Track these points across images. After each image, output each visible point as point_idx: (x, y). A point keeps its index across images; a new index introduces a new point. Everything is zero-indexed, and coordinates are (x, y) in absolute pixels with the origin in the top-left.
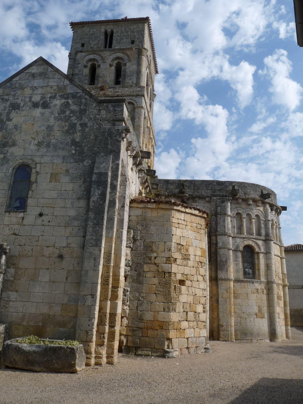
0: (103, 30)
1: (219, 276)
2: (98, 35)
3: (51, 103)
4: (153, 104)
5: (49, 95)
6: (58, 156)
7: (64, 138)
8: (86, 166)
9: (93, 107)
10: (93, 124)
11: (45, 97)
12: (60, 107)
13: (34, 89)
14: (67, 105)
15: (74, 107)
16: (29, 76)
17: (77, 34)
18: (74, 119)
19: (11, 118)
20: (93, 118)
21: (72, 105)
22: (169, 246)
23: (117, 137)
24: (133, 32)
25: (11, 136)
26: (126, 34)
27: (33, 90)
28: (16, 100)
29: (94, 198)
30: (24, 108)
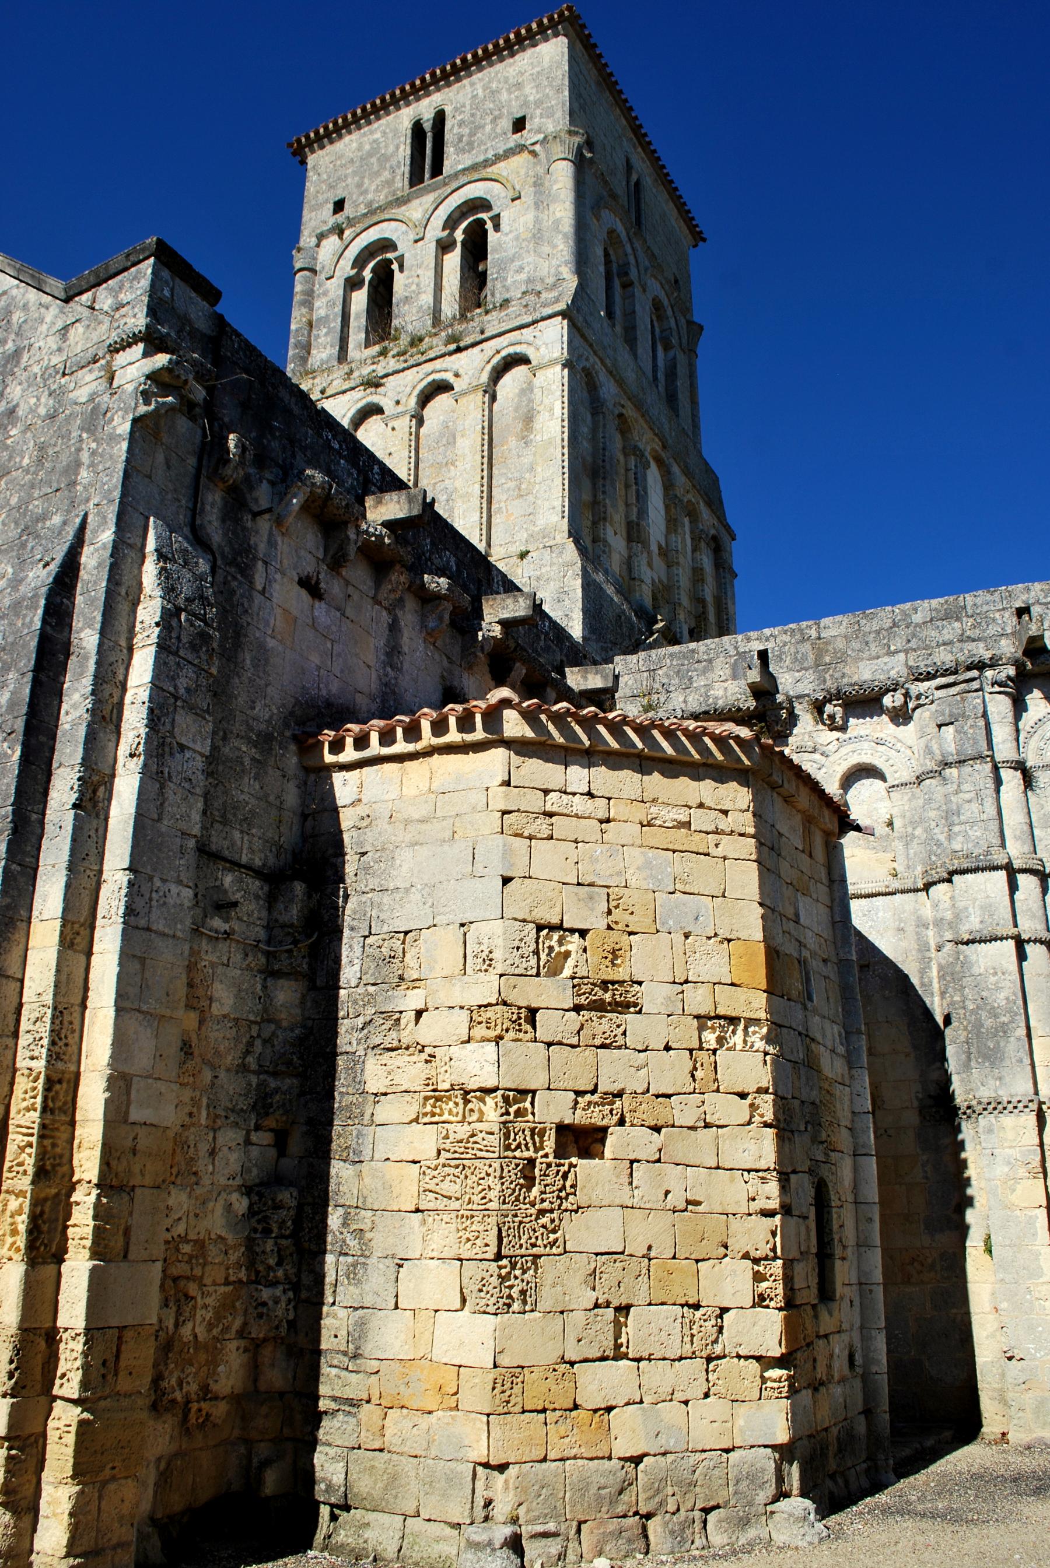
2: (391, 148)
4: (692, 375)
20: (39, 376)
22: (486, 941)
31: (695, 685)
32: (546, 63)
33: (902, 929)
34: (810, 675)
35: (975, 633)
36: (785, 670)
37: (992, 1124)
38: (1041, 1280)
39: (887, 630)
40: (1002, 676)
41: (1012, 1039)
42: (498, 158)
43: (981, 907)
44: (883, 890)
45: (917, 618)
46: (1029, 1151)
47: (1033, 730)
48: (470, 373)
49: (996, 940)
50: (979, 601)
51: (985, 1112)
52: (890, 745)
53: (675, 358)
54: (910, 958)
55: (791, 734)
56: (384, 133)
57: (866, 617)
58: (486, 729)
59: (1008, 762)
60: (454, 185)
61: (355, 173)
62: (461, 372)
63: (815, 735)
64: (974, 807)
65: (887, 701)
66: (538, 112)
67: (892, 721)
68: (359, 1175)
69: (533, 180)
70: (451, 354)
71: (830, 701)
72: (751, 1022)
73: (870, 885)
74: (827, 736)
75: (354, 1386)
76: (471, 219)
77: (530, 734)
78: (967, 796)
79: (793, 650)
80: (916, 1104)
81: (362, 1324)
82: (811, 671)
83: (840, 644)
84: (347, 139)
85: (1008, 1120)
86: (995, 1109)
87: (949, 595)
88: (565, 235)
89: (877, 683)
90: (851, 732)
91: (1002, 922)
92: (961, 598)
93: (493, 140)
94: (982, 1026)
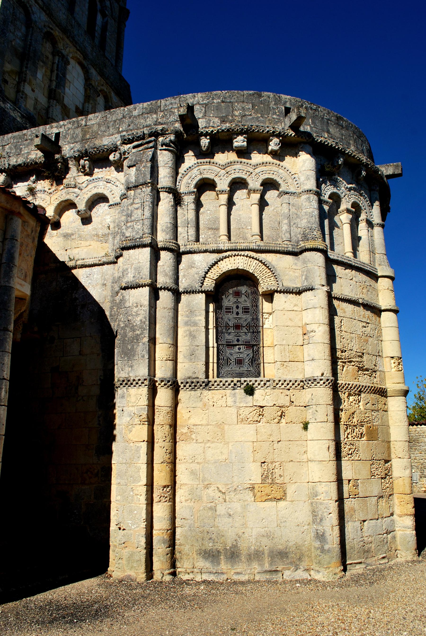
31: (23, 153)
33: (105, 284)
36: (67, 143)
37: (124, 393)
38: (139, 484)
39: (120, 120)
41: (141, 344)
43: (135, 269)
44: (97, 262)
45: (135, 113)
46: (141, 409)
47: (185, 173)
49: (139, 287)
51: (121, 386)
52: (113, 183)
53: (107, 21)
54: (107, 300)
55: (65, 178)
57: (110, 113)
59: (164, 188)
63: (76, 178)
64: (139, 212)
67: (116, 169)
71: (82, 158)
73: (92, 260)
74: (83, 179)
79: (72, 132)
80: (99, 382)
82: (79, 143)
83: (95, 128)
85: (133, 391)
86: (126, 384)
87: (153, 100)
89: (106, 147)
90: (94, 176)
91: (144, 276)
92: (159, 102)
94: (126, 336)
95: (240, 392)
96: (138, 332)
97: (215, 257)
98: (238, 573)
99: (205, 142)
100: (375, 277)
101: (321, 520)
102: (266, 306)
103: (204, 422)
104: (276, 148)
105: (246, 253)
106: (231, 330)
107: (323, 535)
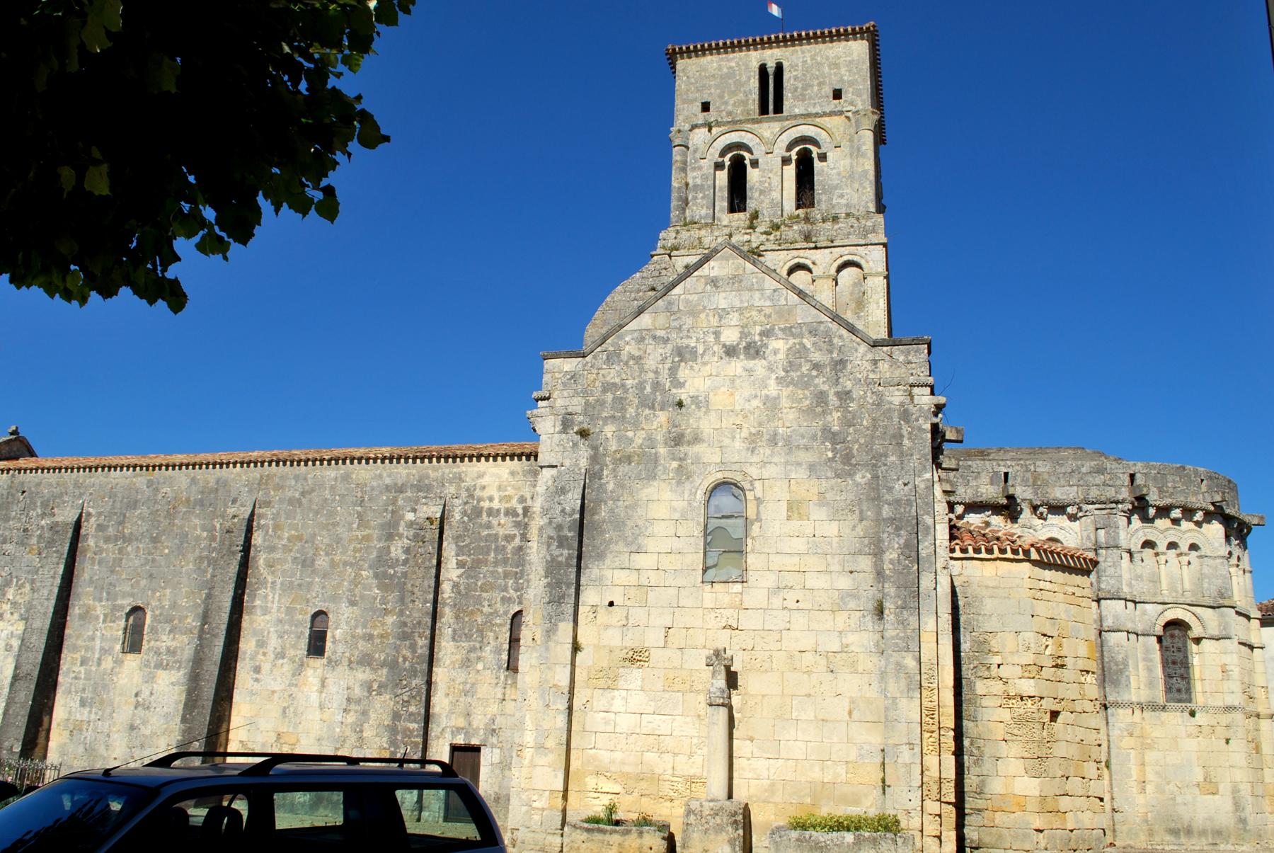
0: (755, 65)
1: (1111, 698)
2: (744, 78)
3: (766, 346)
5: (758, 329)
6: (799, 464)
7: (805, 424)
8: (860, 484)
9: (859, 355)
10: (865, 393)
11: (750, 333)
12: (787, 355)
13: (722, 314)
14: (801, 352)
15: (817, 357)
16: (706, 284)
17: (688, 77)
18: (821, 383)
19: (682, 380)
21: (812, 350)
23: (920, 422)
24: (837, 66)
25: (688, 420)
26: (817, 73)
27: (721, 317)
28: (686, 341)
29: (891, 553)
30: (706, 358)
32: (855, 56)
34: (1030, 490)
35: (1111, 483)
40: (1126, 509)
42: (825, 114)
45: (1084, 470)
48: (824, 265)
50: (1113, 467)
56: (738, 64)
58: (1024, 555)
60: (795, 123)
61: (717, 87)
62: (817, 262)
65: (1069, 510)
66: (851, 90)
68: (977, 726)
69: (849, 137)
70: (810, 249)
71: (1042, 506)
72: (1093, 673)
75: (980, 804)
76: (802, 147)
77: (1039, 558)
78: (1109, 564)
81: (983, 782)
83: (1046, 476)
84: (709, 58)
88: (870, 181)
90: (1049, 521)
93: (819, 98)
95: (1186, 714)
96: (1121, 667)
97: (1161, 607)
98: (1193, 845)
99: (1152, 512)
100: (1248, 618)
101: (1243, 809)
102: (1194, 647)
103: (1163, 736)
104: (1200, 519)
105: (1183, 606)
106: (1170, 665)
107: (1245, 820)
